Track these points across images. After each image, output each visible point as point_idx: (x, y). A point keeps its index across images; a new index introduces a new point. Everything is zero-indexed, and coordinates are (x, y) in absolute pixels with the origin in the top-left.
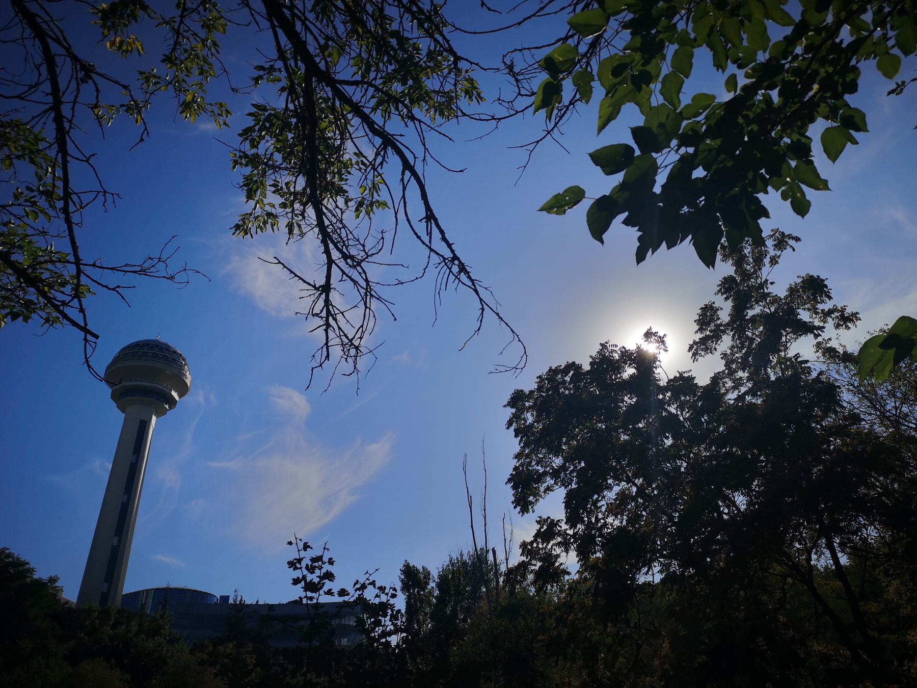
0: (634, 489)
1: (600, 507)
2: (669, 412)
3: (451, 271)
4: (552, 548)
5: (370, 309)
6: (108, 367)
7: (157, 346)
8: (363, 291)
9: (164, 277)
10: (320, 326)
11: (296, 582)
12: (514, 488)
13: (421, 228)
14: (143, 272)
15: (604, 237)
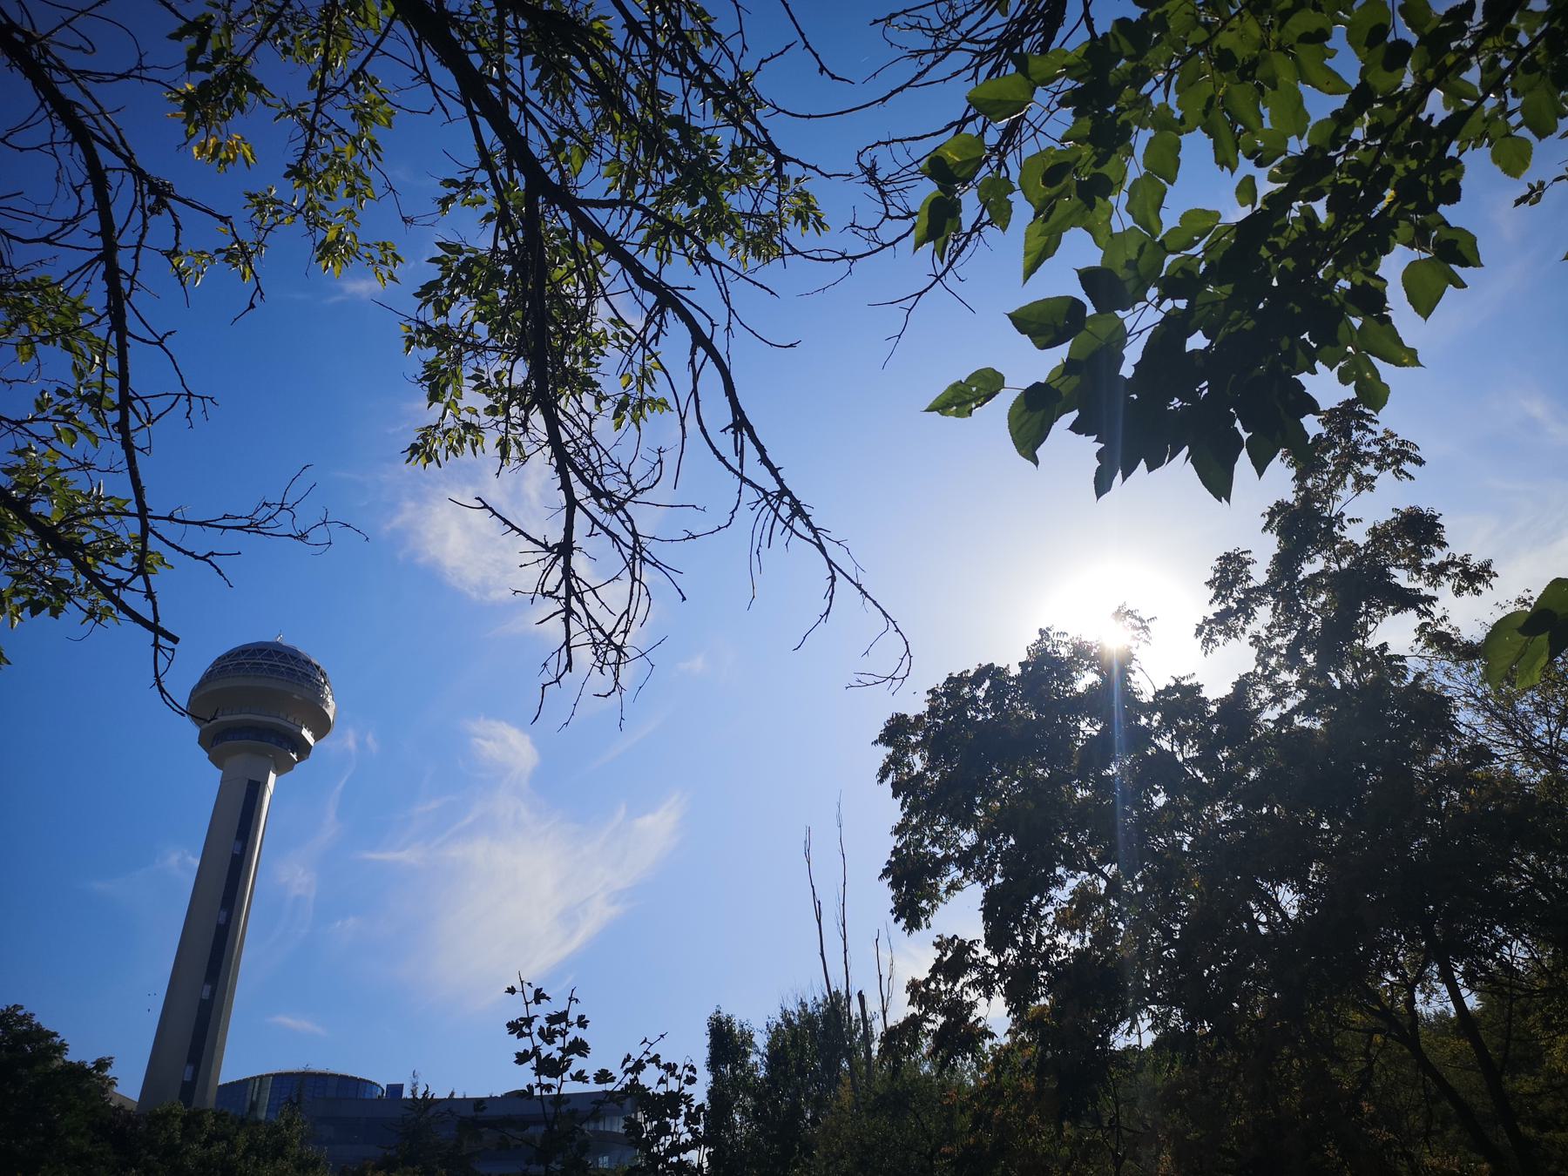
0: (1103, 883)
2: (1159, 749)
3: (777, 515)
4: (962, 990)
6: (194, 691)
7: (278, 653)
9: (290, 535)
10: (555, 614)
11: (522, 1058)
12: (893, 885)
13: (725, 443)
14: (254, 527)
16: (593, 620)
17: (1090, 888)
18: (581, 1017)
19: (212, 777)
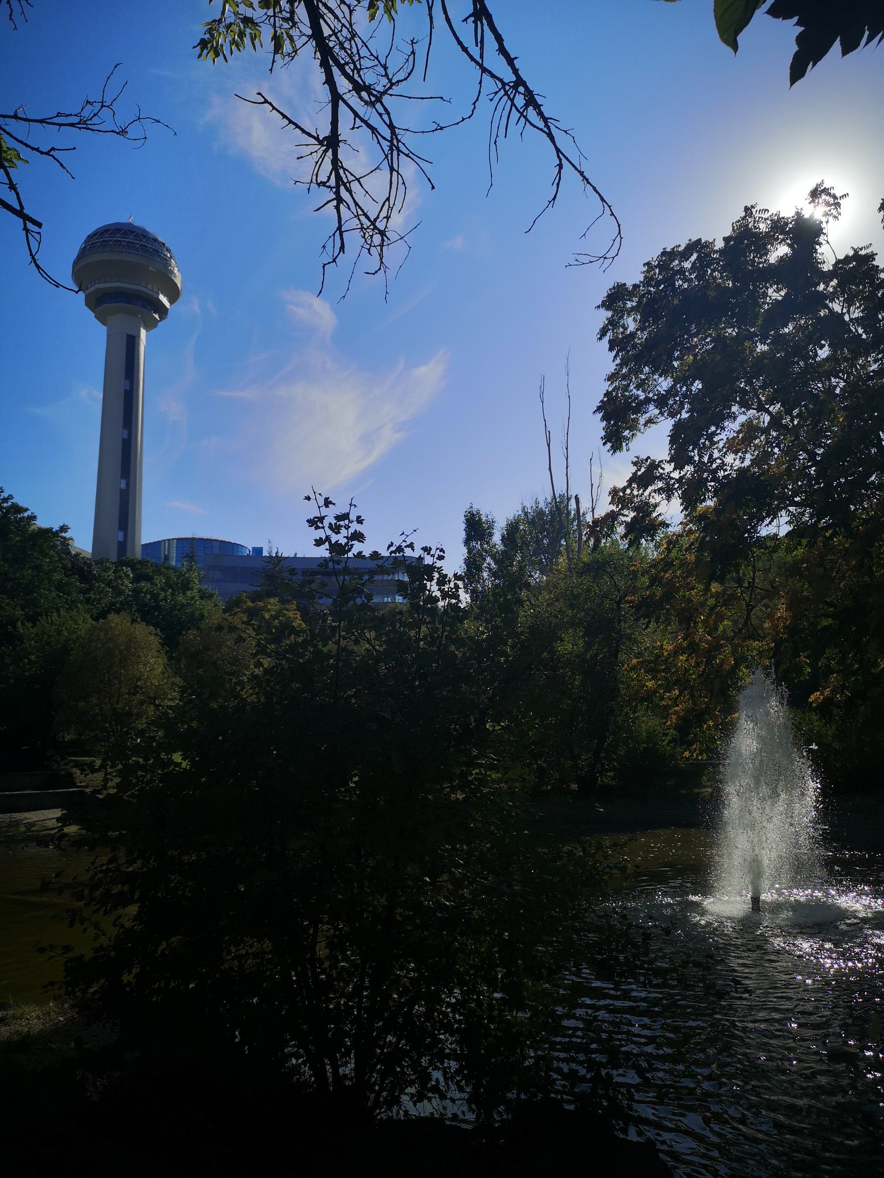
0: (767, 418)
1: (718, 442)
2: (831, 311)
3: (513, 104)
4: (649, 495)
5: (398, 174)
6: (75, 263)
7: (132, 232)
8: (385, 145)
9: (113, 131)
10: (328, 202)
11: (319, 542)
12: (603, 418)
13: (467, 32)
14: (83, 124)
15: (740, 38)
16: (360, 208)
17: (755, 422)
18: (358, 517)
19: (102, 330)
